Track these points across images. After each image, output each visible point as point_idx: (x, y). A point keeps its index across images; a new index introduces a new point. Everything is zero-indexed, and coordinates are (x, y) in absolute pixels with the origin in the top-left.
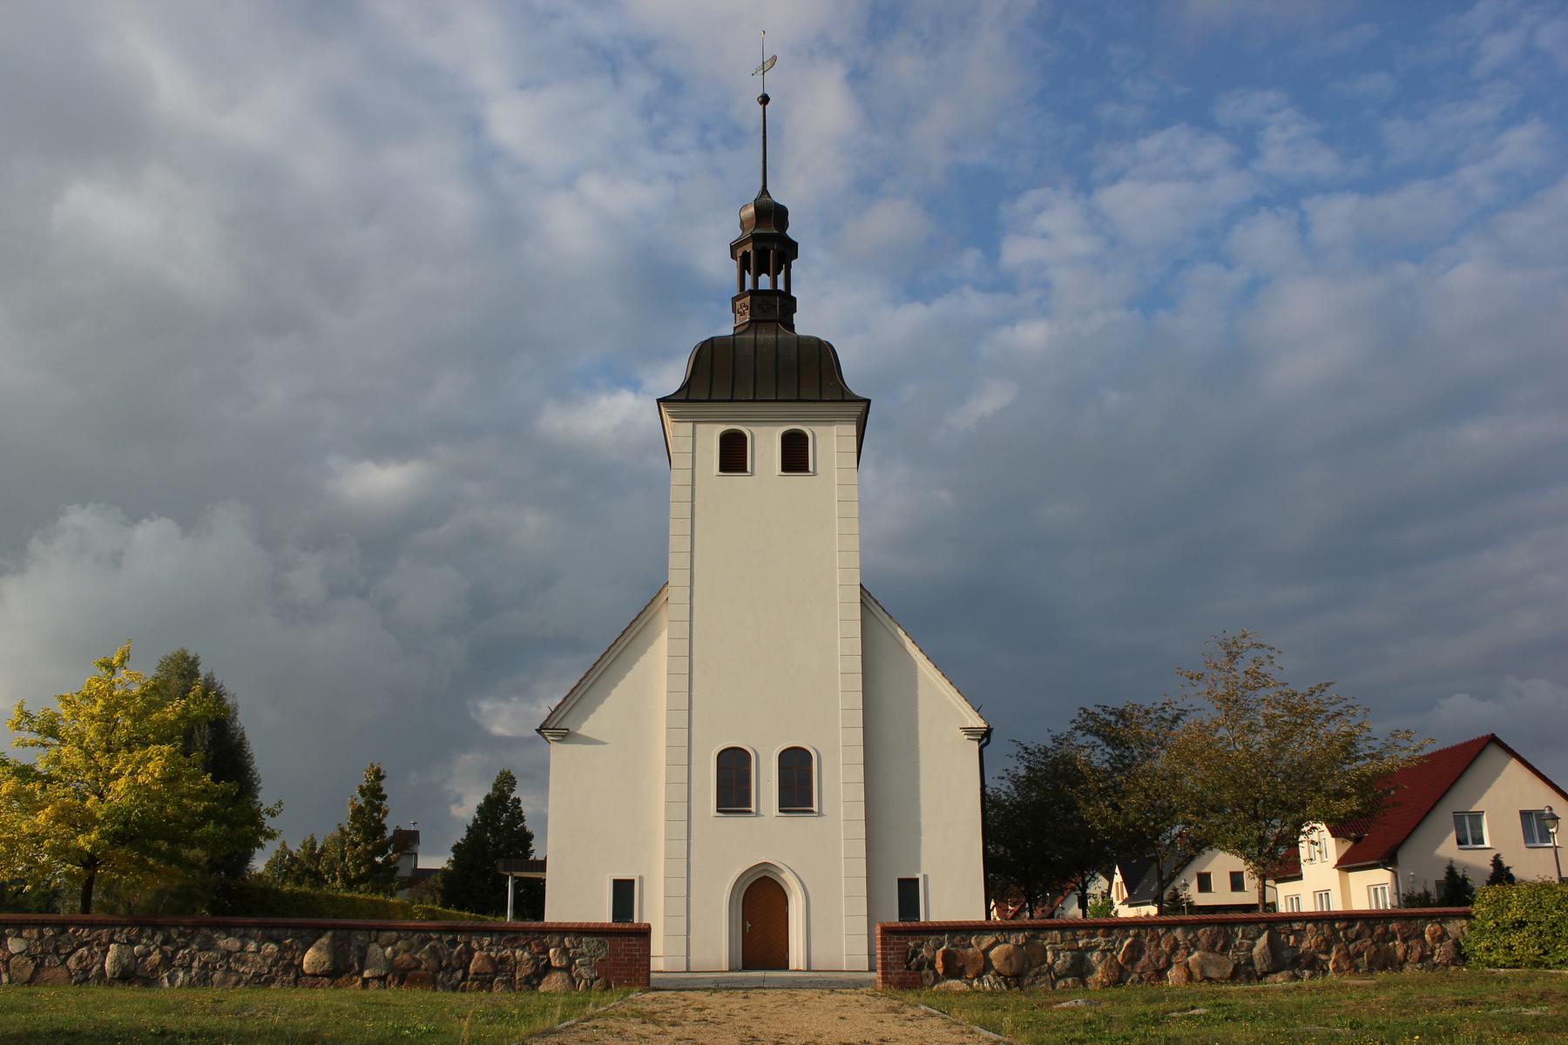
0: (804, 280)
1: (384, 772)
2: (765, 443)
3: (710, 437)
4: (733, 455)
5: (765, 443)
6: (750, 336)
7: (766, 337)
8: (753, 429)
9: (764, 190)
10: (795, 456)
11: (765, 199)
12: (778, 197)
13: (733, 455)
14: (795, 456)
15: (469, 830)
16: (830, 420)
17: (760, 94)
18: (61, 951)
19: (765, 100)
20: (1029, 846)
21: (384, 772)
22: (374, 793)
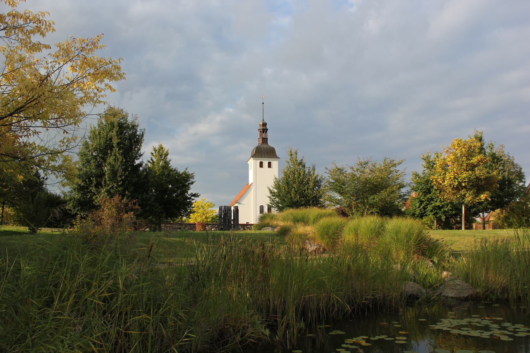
0: (270, 135)
1: (513, 157)
2: (265, 164)
3: (258, 162)
4: (261, 165)
5: (265, 164)
6: (262, 146)
7: (265, 146)
8: (265, 161)
9: (263, 120)
10: (270, 165)
11: (264, 122)
12: (266, 121)
13: (261, 165)
14: (270, 165)
15: (185, 173)
16: (274, 160)
17: (228, 205)
18: (186, 239)
19: (263, 103)
20: (459, 217)
21: (513, 157)
22: (302, 160)
